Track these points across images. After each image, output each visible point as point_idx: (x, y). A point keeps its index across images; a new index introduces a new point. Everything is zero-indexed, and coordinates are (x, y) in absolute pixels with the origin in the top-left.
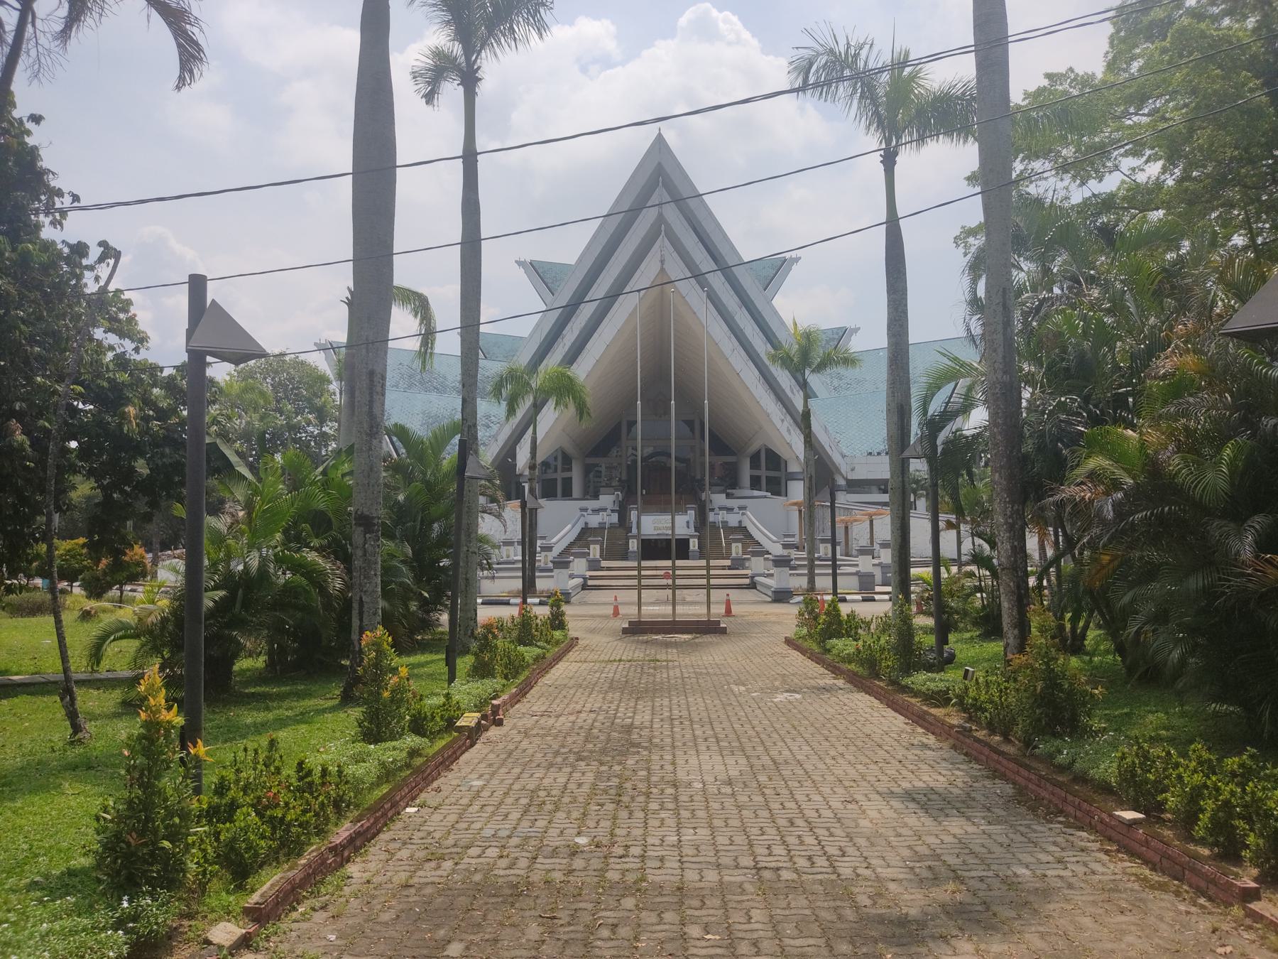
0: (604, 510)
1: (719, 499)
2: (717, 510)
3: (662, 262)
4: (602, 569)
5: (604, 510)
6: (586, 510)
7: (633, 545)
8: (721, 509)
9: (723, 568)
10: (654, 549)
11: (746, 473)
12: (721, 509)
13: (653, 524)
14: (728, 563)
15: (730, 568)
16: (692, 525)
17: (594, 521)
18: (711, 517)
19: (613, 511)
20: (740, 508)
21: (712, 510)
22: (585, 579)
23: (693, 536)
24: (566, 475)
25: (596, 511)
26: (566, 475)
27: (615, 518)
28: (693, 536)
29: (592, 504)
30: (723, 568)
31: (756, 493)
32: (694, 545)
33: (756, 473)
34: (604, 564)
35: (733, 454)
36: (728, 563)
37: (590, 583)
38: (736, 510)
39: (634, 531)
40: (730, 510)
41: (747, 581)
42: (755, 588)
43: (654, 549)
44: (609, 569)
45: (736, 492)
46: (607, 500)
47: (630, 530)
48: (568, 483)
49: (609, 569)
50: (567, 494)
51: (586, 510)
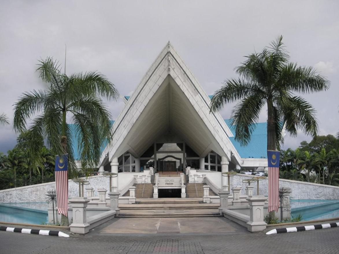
11: (203, 164)
33: (206, 164)
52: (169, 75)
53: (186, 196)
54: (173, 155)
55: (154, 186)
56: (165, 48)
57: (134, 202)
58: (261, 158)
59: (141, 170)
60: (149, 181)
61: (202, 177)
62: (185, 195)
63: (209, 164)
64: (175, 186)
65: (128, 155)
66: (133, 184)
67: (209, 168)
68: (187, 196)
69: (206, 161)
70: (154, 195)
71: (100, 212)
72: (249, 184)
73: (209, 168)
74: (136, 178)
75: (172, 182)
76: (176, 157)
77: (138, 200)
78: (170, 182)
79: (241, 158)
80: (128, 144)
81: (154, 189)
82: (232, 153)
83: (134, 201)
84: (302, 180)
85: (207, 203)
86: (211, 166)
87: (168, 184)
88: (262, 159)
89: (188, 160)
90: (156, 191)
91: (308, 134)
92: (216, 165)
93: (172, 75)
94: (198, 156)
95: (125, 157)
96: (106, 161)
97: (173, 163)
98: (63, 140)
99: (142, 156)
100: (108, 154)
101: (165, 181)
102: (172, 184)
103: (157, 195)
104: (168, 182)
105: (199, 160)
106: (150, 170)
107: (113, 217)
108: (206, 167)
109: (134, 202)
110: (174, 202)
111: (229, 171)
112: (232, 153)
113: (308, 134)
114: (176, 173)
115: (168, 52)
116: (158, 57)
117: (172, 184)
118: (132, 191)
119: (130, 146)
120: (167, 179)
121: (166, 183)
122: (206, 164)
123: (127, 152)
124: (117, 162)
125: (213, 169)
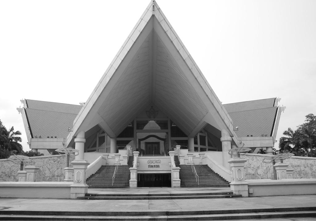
11: (192, 145)
33: (196, 146)
53: (181, 185)
54: (156, 134)
55: (131, 168)
57: (83, 195)
58: (262, 136)
60: (125, 162)
61: (199, 157)
62: (180, 182)
63: (199, 146)
64: (162, 170)
66: (14, 128)
67: (199, 149)
68: (183, 185)
69: (196, 143)
70: (130, 183)
72: (282, 162)
73: (199, 149)
74: (107, 158)
75: (157, 164)
77: (91, 191)
78: (155, 164)
79: (238, 137)
81: (131, 174)
83: (82, 193)
85: (243, 196)
87: (152, 166)
88: (263, 137)
90: (133, 177)
93: (157, 16)
94: (186, 136)
97: (156, 145)
101: (147, 164)
102: (158, 166)
103: (136, 183)
104: (152, 164)
105: (187, 140)
106: (126, 149)
109: (83, 195)
110: (171, 195)
116: (142, 19)
117: (158, 166)
118: (80, 171)
120: (151, 159)
121: (149, 166)
122: (196, 146)
124: (83, 138)
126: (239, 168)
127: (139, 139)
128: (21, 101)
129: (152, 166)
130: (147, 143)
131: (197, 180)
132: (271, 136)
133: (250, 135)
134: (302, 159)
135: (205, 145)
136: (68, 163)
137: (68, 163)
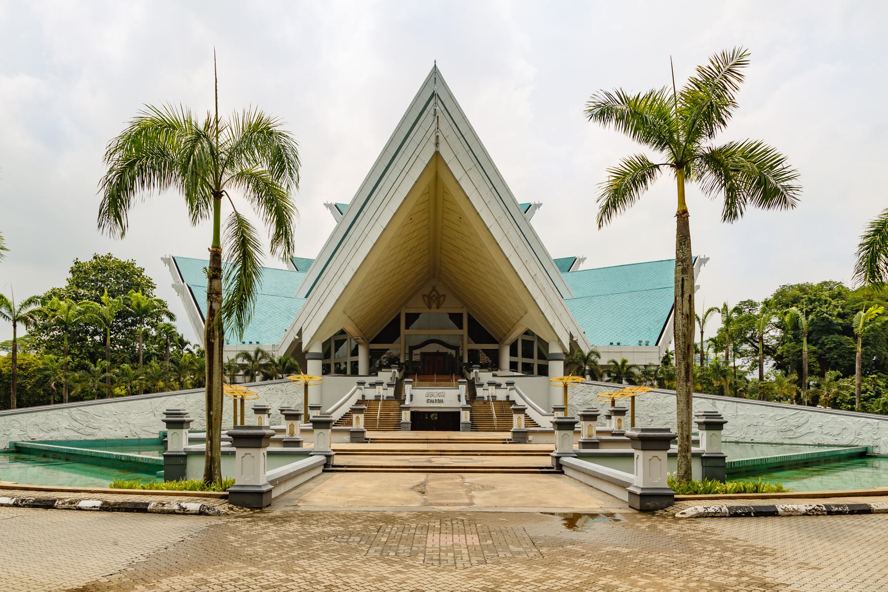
0: (381, 384)
1: (485, 376)
2: (486, 386)
3: (437, 144)
4: (366, 441)
5: (381, 384)
6: (363, 384)
7: (406, 417)
8: (490, 384)
9: (504, 441)
10: (422, 421)
11: (506, 358)
12: (490, 384)
13: (422, 396)
14: (508, 435)
15: (510, 441)
16: (463, 398)
17: (371, 394)
18: (480, 392)
19: (389, 385)
20: (508, 384)
21: (481, 385)
22: (329, 457)
23: (464, 409)
24: (354, 359)
25: (373, 385)
26: (354, 359)
27: (391, 392)
28: (464, 409)
29: (373, 379)
30: (504, 441)
31: (515, 374)
32: (465, 417)
33: (514, 359)
34: (369, 435)
35: (494, 342)
36: (508, 435)
37: (338, 460)
38: (504, 386)
39: (407, 402)
40: (498, 386)
41: (547, 461)
42: (562, 473)
43: (422, 421)
44: (374, 441)
45: (498, 373)
46: (385, 376)
47: (403, 402)
48: (355, 365)
49: (374, 441)
50: (355, 372)
51: (363, 384)
52: (437, 153)
56: (426, 84)
59: (373, 371)
60: (408, 389)
63: (520, 360)
65: (342, 337)
67: (520, 366)
69: (513, 353)
71: (289, 459)
73: (520, 366)
76: (437, 345)
80: (345, 313)
82: (571, 337)
84: (738, 157)
86: (523, 364)
87: (432, 401)
89: (472, 350)
91: (713, 63)
92: (535, 362)
95: (336, 342)
96: (296, 345)
98: (44, 303)
99: (374, 341)
100: (300, 334)
102: (441, 401)
105: (497, 350)
107: (320, 470)
108: (513, 366)
111: (565, 375)
112: (571, 337)
113: (713, 63)
114: (448, 377)
115: (433, 95)
117: (441, 401)
119: (349, 317)
122: (514, 359)
123: (342, 332)
125: (528, 370)
126: (629, 413)
127: (410, 347)
128: (162, 259)
129: (432, 401)
130: (423, 355)
131: (495, 423)
132: (657, 344)
133: (615, 343)
134: (834, 446)
135: (516, 355)
136: (15, 351)
137: (15, 351)
